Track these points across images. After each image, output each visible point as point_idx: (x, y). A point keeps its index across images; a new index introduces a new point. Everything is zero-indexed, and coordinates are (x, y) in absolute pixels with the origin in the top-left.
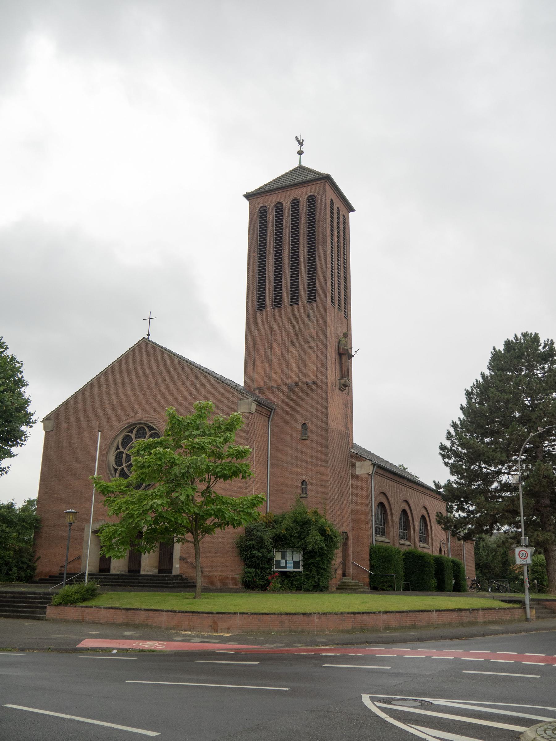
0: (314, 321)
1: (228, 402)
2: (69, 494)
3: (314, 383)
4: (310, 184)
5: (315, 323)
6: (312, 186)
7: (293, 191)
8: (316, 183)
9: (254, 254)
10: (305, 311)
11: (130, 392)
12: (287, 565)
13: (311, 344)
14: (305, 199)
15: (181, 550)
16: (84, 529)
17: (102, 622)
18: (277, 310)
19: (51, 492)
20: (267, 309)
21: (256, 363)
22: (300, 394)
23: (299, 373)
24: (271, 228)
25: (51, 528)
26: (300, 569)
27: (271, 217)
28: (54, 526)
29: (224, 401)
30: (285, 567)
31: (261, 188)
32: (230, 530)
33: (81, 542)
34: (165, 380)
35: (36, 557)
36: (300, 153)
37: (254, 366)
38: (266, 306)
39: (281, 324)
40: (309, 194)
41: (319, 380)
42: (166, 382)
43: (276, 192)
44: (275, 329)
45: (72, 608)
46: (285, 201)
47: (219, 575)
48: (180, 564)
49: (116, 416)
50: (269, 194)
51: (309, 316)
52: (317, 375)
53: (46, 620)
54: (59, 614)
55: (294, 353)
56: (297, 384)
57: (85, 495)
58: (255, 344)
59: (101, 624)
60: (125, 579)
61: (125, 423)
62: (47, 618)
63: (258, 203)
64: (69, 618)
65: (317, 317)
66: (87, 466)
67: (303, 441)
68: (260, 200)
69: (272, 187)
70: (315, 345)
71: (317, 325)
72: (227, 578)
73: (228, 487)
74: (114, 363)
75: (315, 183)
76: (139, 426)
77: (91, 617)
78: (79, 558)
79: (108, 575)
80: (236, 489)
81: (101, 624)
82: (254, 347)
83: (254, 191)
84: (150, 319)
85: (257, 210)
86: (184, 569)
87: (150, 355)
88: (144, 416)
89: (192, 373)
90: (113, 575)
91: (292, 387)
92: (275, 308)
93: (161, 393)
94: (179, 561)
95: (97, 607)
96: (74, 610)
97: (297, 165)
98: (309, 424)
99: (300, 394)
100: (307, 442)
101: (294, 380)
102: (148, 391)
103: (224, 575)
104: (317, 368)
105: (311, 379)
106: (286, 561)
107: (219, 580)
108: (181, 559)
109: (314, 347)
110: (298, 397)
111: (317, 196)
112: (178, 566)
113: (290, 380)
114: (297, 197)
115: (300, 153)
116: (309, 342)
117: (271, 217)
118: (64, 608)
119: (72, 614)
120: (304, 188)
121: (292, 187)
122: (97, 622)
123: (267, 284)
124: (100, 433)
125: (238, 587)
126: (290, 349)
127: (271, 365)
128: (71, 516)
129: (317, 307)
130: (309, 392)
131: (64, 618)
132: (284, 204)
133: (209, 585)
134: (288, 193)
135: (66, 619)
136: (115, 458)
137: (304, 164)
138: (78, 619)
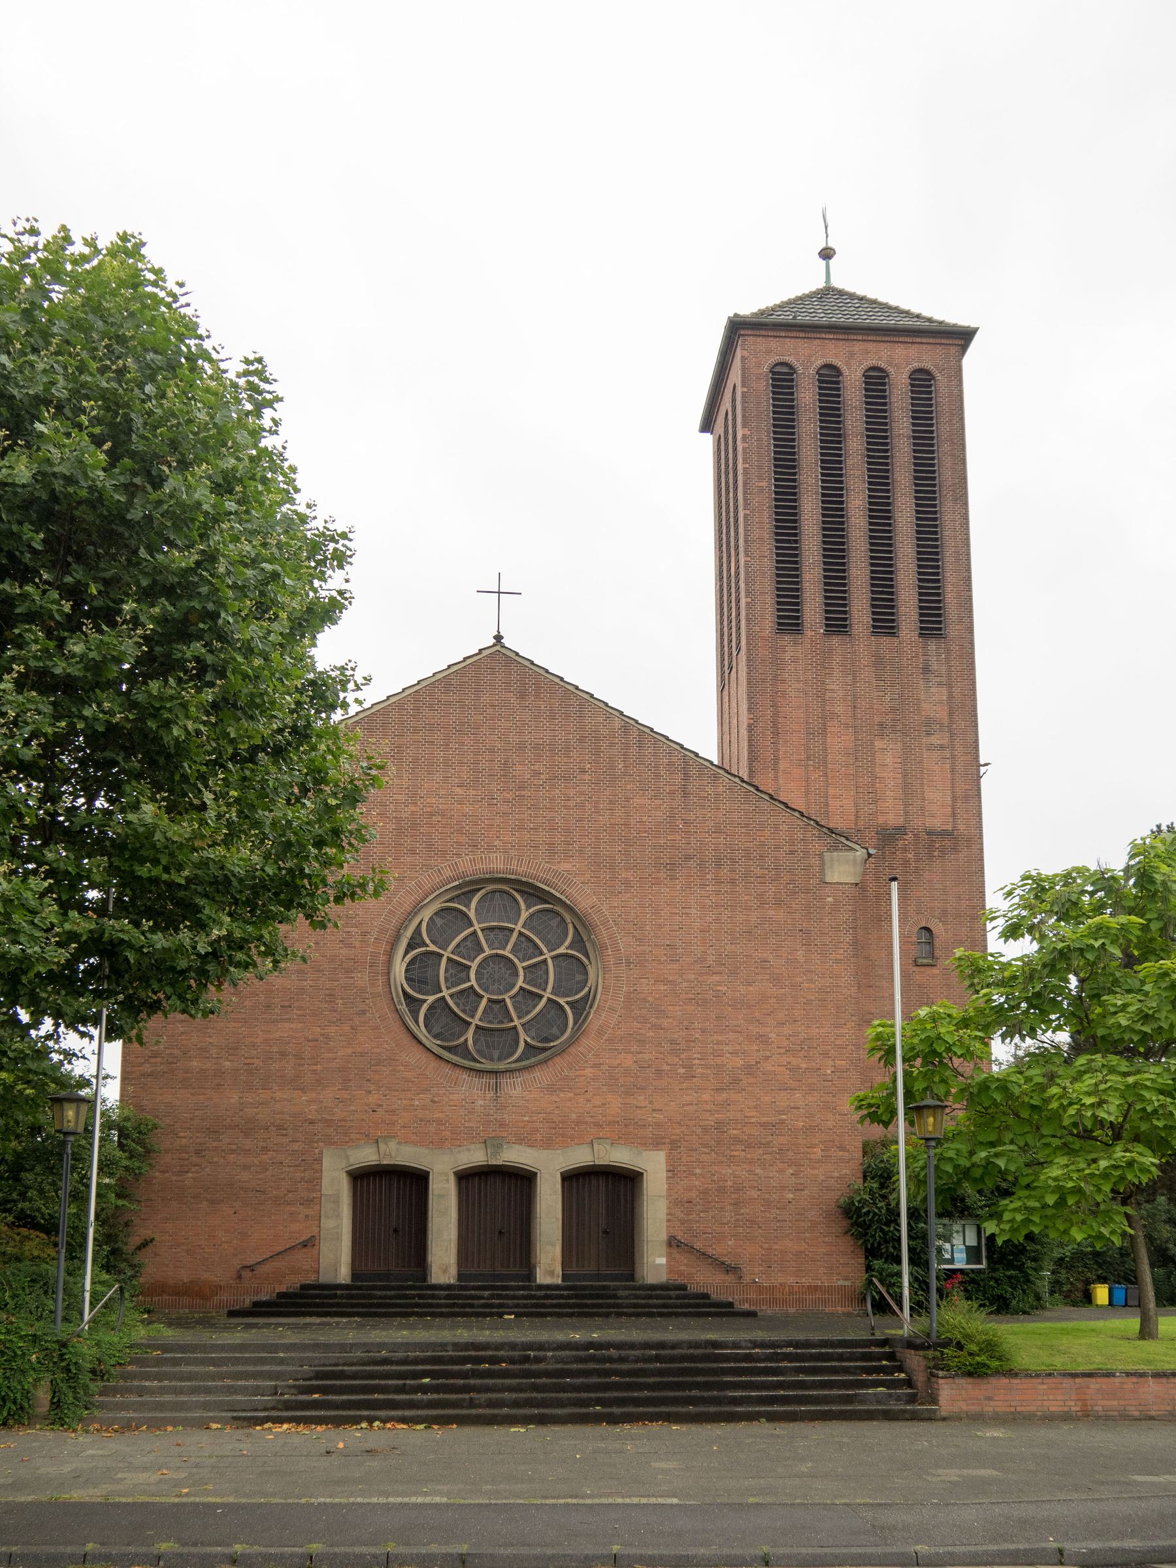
0: (940, 684)
1: (792, 852)
2: (252, 1061)
3: (944, 834)
4: (918, 340)
5: (944, 691)
6: (924, 347)
7: (871, 346)
8: (938, 341)
9: (764, 484)
10: (916, 656)
11: (458, 790)
12: (956, 1255)
13: (935, 740)
14: (906, 375)
15: (668, 1221)
16: (319, 1161)
17: (1153, 1413)
18: (835, 641)
19: (176, 1052)
20: (809, 633)
21: (782, 765)
22: (910, 856)
23: (906, 805)
24: (808, 428)
25: (185, 1156)
26: (980, 1263)
27: (807, 396)
28: (198, 1152)
29: (777, 848)
30: (951, 1261)
31: (762, 313)
32: (816, 1172)
33: (313, 1199)
34: (583, 771)
35: (135, 1241)
36: (827, 254)
37: (775, 769)
38: (807, 625)
39: (850, 677)
40: (916, 365)
41: (961, 827)
42: (587, 777)
43: (824, 336)
44: (832, 687)
45: (1040, 1380)
46: (848, 364)
47: (791, 1280)
48: (669, 1256)
49: (413, 852)
50: (802, 335)
51: (926, 670)
52: (954, 814)
53: (944, 1419)
54: (990, 1399)
55: (888, 754)
56: (901, 830)
57: (314, 1067)
58: (776, 714)
59: (1152, 1418)
60: (568, 1297)
61: (448, 873)
62: (944, 1414)
63: (768, 352)
64: (1033, 1408)
65: (949, 676)
66: (311, 983)
67: (922, 969)
68: (773, 344)
69: (804, 318)
70: (945, 742)
71: (951, 696)
72: (816, 1288)
73: (804, 1066)
74: (392, 700)
75: (931, 340)
76: (491, 887)
77: (1115, 1403)
78: (309, 1243)
79: (634, 1288)
80: (829, 1072)
81: (1152, 1418)
82: (775, 724)
83: (754, 315)
84: (499, 593)
85: (766, 368)
86: (683, 1268)
87: (522, 696)
88: (515, 862)
89: (671, 764)
90: (541, 1287)
91: (889, 837)
92: (828, 633)
93: (571, 804)
94: (664, 1249)
95: (1128, 1374)
96: (1045, 1387)
97: (821, 285)
98: (938, 928)
99: (910, 856)
100: (935, 971)
101: (892, 818)
102: (525, 793)
103: (806, 1281)
104: (954, 798)
105: (937, 823)
106: (952, 1246)
107: (791, 1293)
108: (673, 1243)
109: (942, 747)
110: (906, 862)
111: (939, 376)
112: (662, 1261)
113: (881, 820)
114: (882, 365)
115: (827, 254)
116: (928, 734)
117: (807, 396)
118: (1007, 1381)
119: (1040, 1398)
120: (902, 346)
121: (868, 335)
122: (1137, 1414)
123: (805, 569)
124: (894, 885)
125: (846, 1310)
126: (879, 744)
127: (826, 775)
128: (931, 1120)
129: (948, 652)
130: (936, 854)
131: (1013, 1409)
132: (845, 371)
133: (764, 1308)
134: (856, 349)
135: (1019, 1413)
136: (407, 971)
137: (837, 283)
138: (1067, 1409)
